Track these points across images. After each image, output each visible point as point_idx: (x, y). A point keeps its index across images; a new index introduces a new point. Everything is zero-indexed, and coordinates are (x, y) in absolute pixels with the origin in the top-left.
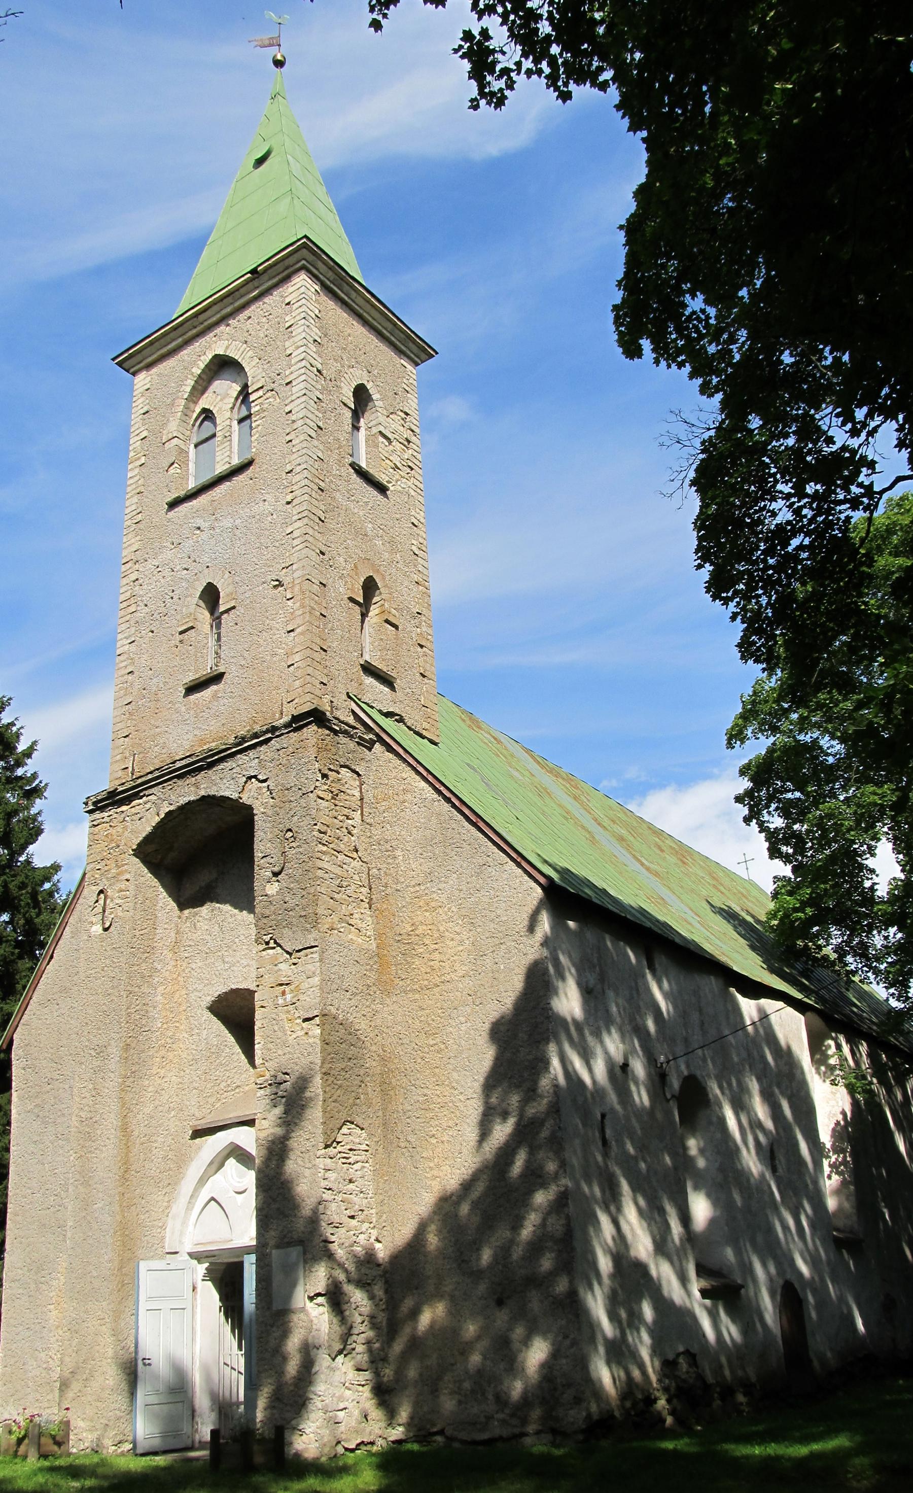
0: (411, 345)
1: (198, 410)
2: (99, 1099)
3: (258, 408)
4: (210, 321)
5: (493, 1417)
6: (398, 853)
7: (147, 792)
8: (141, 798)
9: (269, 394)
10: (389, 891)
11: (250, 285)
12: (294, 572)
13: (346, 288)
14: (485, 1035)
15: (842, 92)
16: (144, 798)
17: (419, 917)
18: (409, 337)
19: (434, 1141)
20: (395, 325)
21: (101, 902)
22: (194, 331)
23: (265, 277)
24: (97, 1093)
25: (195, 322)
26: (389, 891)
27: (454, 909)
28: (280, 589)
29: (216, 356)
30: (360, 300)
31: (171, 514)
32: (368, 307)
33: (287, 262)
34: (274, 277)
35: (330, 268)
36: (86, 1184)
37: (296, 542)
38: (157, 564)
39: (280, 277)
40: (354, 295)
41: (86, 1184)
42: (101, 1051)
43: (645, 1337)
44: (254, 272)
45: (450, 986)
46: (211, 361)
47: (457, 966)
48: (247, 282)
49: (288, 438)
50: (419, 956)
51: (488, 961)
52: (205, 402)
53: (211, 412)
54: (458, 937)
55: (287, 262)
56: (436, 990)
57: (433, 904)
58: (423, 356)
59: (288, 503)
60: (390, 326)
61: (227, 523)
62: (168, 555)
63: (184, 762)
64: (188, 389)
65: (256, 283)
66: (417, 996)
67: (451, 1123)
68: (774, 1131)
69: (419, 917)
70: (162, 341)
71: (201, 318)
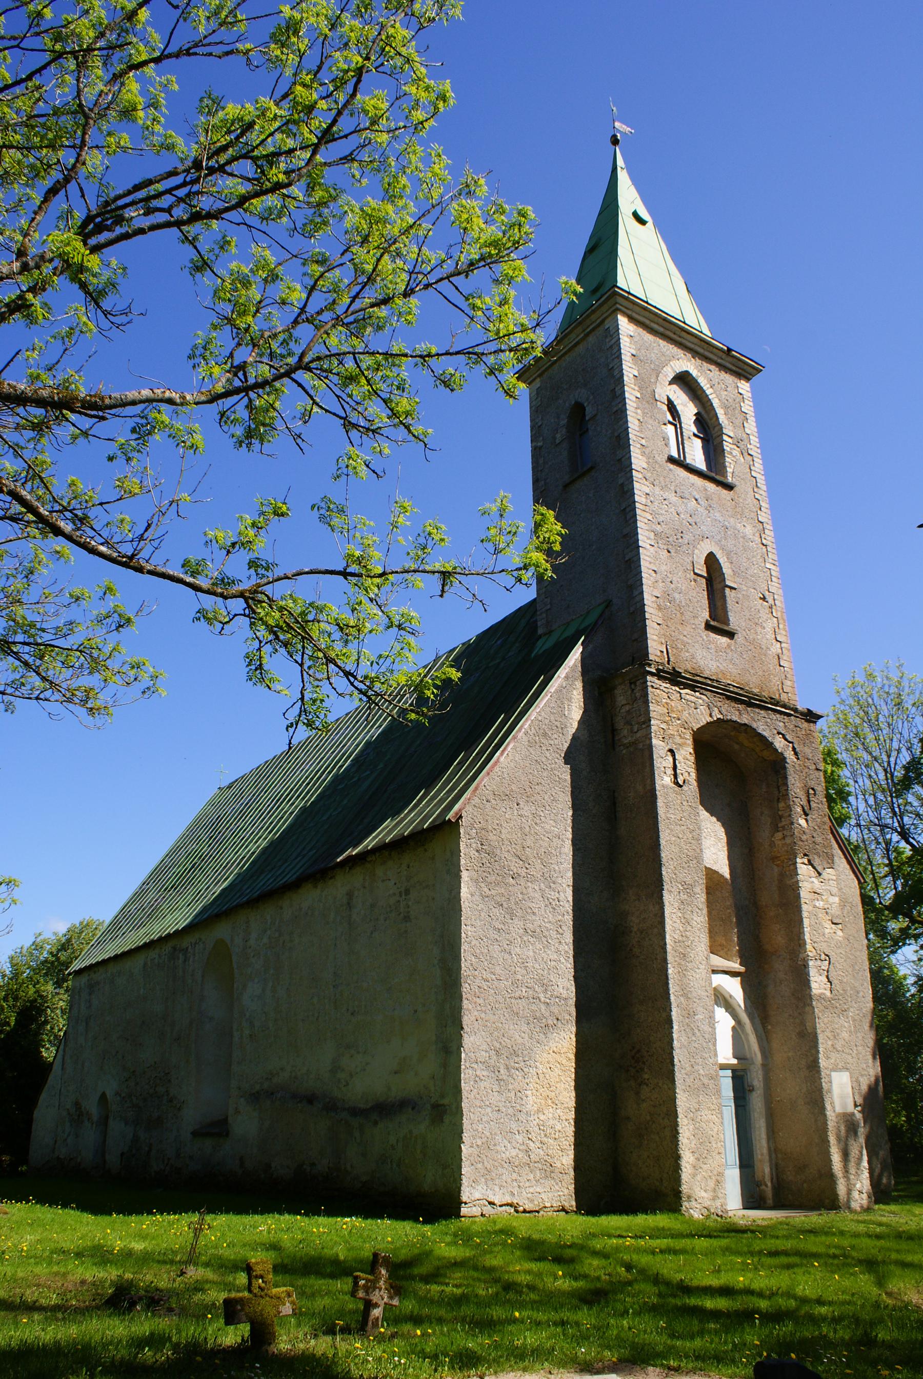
2: (689, 928)
4: (684, 341)
7: (702, 691)
8: (695, 691)
11: (721, 353)
14: (561, 762)
16: (697, 694)
23: (730, 359)
25: (678, 331)
34: (734, 365)
38: (648, 492)
39: (737, 370)
43: (29, 515)
44: (729, 350)
48: (721, 350)
55: (746, 367)
63: (736, 690)
65: (724, 356)
68: (727, 875)
71: (684, 334)
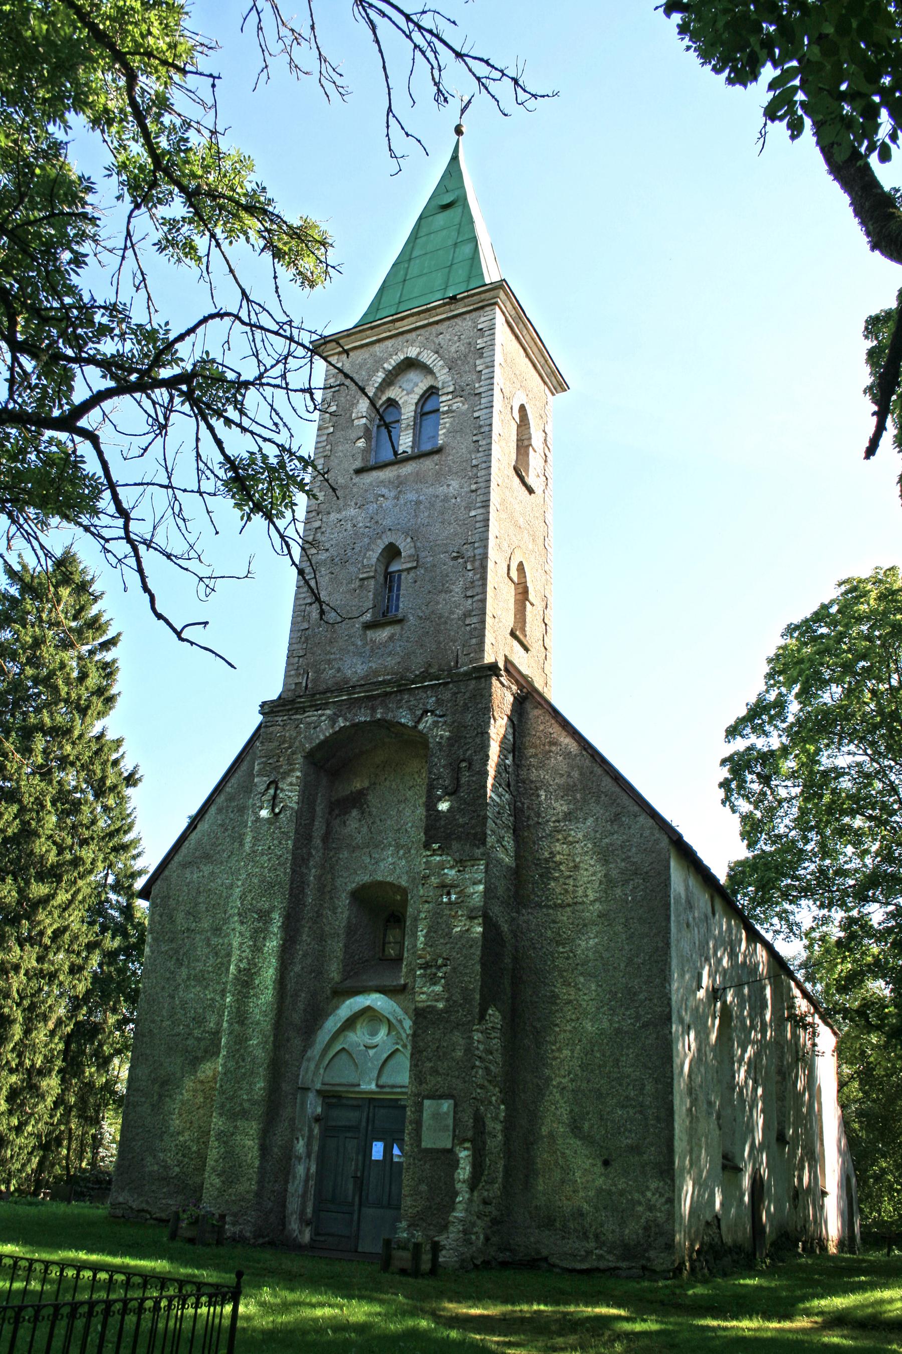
0: (553, 379)
1: (384, 398)
3: (446, 408)
5: (592, 1252)
6: (542, 793)
9: (459, 399)
10: (531, 822)
12: (475, 549)
13: (521, 325)
15: (874, 102)
17: (558, 847)
18: (553, 372)
19: (557, 1029)
20: (546, 361)
21: (272, 791)
22: (388, 334)
24: (257, 949)
26: (531, 822)
27: (590, 846)
28: (460, 560)
29: (407, 358)
30: (528, 337)
31: (356, 479)
32: (532, 344)
33: (483, 296)
35: (514, 308)
36: (242, 1023)
37: (478, 525)
40: (525, 332)
41: (242, 1023)
42: (264, 916)
45: (580, 907)
46: (403, 361)
47: (589, 892)
49: (475, 438)
50: (556, 879)
51: (618, 891)
52: (392, 393)
53: (397, 402)
54: (591, 869)
56: (568, 909)
57: (570, 839)
58: (559, 389)
59: (472, 491)
60: (543, 362)
61: (412, 496)
62: (352, 511)
64: (380, 380)
65: (452, 307)
66: (551, 911)
67: (574, 1017)
69: (558, 847)
70: (358, 336)
